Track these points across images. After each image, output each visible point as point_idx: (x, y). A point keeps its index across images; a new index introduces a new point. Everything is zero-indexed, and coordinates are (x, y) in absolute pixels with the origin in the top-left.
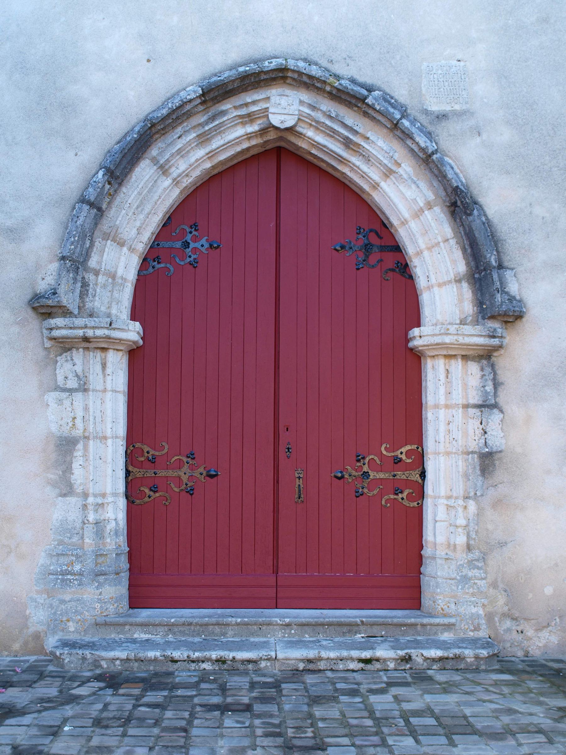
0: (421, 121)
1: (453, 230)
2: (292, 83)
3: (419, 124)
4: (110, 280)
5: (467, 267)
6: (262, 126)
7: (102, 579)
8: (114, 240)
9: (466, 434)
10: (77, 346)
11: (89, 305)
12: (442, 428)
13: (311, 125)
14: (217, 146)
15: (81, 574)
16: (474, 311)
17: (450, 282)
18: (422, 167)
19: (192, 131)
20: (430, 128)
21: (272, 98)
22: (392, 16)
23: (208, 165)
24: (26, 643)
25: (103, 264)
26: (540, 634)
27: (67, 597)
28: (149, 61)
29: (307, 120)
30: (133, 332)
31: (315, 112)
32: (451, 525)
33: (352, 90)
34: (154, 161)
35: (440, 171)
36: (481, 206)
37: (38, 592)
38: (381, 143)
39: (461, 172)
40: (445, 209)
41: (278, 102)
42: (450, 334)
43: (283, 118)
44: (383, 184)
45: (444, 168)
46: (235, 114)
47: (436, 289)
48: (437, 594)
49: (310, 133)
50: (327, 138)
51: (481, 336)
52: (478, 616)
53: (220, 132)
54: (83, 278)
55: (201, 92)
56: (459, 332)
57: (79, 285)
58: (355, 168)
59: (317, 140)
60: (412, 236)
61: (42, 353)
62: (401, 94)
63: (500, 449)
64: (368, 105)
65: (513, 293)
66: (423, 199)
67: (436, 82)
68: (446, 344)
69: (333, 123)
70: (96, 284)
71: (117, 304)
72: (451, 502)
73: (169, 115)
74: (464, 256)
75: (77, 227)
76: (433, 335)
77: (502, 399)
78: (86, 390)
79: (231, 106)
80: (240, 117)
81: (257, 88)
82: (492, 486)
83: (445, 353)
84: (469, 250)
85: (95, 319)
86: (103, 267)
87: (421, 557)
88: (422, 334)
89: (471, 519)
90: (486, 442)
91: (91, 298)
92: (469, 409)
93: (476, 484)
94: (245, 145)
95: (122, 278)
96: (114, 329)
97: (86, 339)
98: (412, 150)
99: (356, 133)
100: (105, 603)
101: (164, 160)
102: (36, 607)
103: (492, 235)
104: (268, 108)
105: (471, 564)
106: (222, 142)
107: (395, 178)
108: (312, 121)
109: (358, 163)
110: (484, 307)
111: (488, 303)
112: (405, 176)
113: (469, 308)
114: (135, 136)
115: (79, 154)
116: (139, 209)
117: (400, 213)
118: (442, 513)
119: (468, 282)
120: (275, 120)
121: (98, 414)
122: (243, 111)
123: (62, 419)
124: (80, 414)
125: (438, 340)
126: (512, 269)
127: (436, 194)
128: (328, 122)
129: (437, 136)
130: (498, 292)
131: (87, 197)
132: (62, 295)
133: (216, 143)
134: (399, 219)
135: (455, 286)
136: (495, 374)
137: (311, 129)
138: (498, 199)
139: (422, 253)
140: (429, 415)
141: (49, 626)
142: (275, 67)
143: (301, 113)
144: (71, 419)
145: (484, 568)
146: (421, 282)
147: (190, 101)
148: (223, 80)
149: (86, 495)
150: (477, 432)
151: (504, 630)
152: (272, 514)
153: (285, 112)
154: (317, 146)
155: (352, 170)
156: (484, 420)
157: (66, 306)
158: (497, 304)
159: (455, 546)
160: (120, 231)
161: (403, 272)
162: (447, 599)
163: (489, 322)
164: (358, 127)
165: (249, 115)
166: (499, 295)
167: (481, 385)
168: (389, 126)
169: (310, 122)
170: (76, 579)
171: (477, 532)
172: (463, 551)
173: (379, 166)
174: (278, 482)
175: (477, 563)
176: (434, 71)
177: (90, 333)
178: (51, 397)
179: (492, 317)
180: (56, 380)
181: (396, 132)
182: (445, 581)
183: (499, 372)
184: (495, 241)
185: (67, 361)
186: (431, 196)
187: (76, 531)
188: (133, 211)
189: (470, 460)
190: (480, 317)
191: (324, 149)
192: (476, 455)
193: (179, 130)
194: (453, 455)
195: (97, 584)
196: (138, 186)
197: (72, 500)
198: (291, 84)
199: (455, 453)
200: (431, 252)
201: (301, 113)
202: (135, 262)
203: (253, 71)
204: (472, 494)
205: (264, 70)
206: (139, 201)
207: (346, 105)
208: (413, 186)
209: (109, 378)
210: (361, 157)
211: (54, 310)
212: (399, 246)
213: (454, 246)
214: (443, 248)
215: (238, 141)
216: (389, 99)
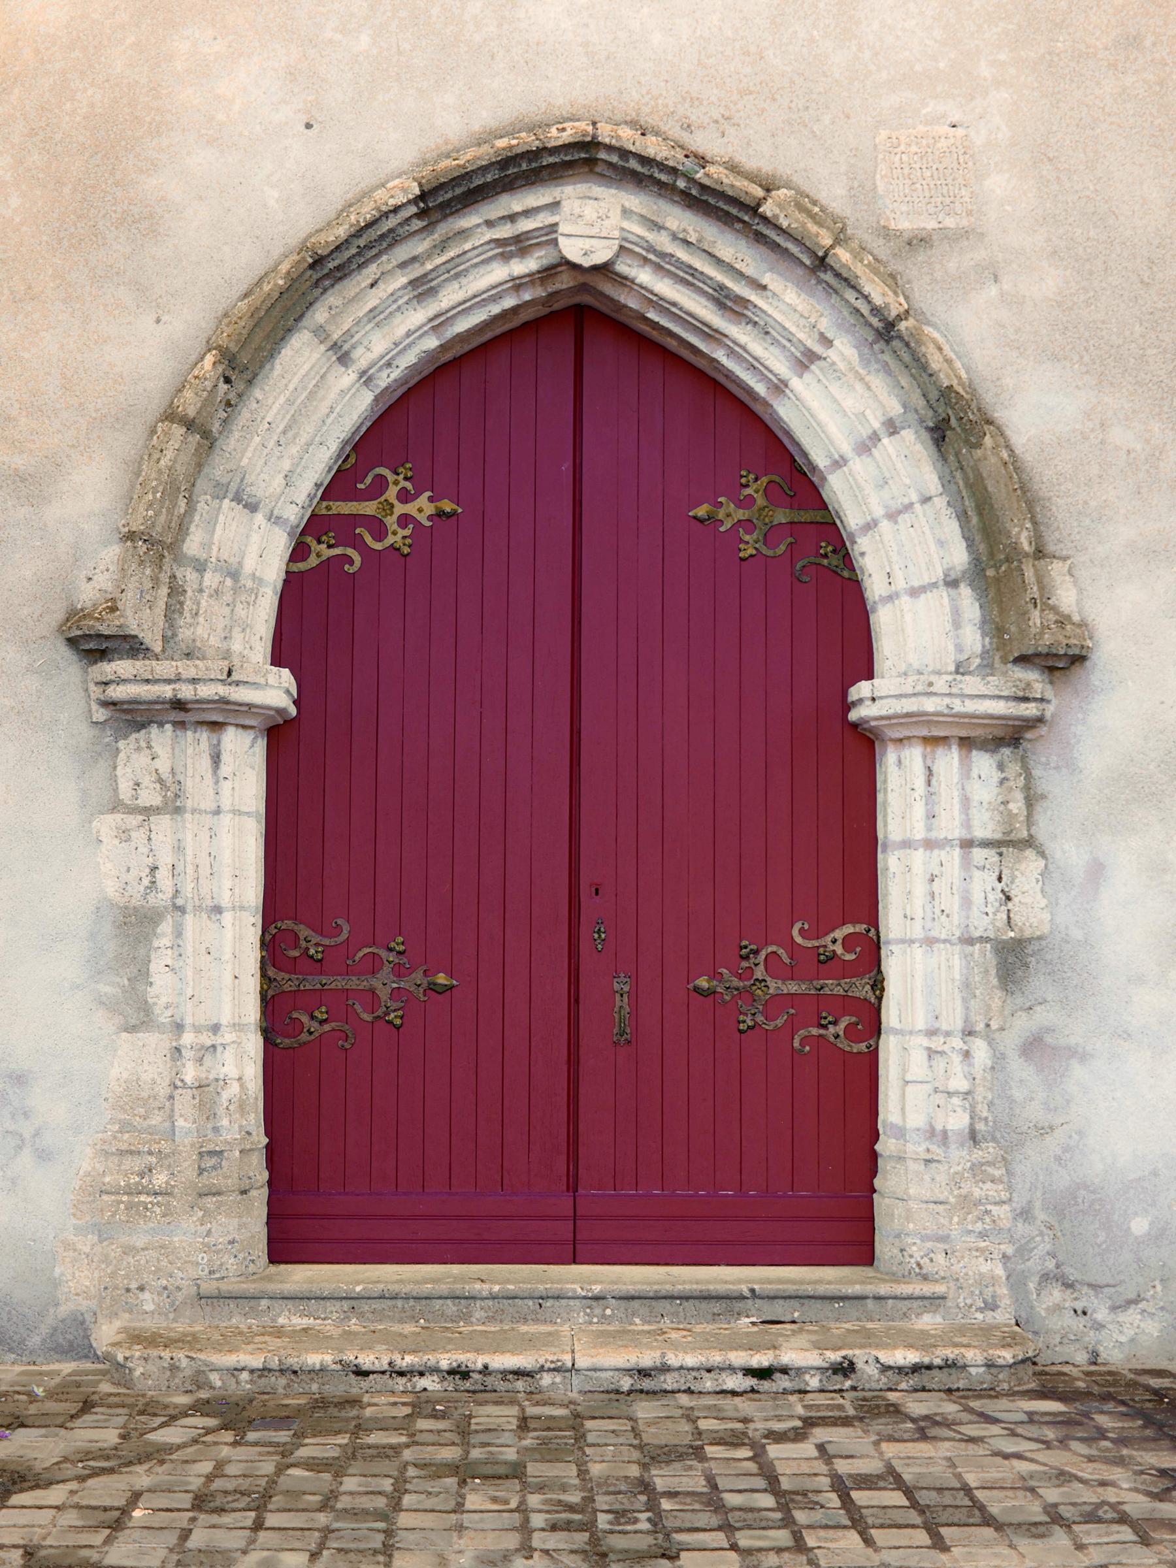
0: (875, 252)
3: (871, 258)
7: (210, 1202)
9: (967, 902)
10: (159, 718)
11: (184, 634)
12: (920, 889)
13: (646, 259)
14: (451, 303)
17: (934, 585)
20: (895, 266)
21: (564, 203)
22: (815, 33)
25: (215, 548)
26: (1122, 1317)
27: (140, 1241)
28: (308, 126)
29: (637, 249)
30: (276, 690)
34: (320, 333)
42: (935, 694)
43: (587, 244)
45: (923, 349)
46: (487, 237)
49: (643, 276)
56: (954, 690)
57: (164, 591)
58: (737, 348)
61: (87, 733)
62: (833, 194)
63: (1038, 933)
67: (906, 171)
68: (926, 714)
72: (937, 1043)
75: (160, 472)
77: (1043, 830)
80: (499, 242)
81: (533, 183)
82: (1021, 1009)
83: (924, 732)
84: (975, 520)
85: (198, 662)
86: (214, 553)
87: (874, 1156)
88: (876, 694)
89: (978, 1077)
90: (1009, 918)
91: (189, 620)
94: (509, 302)
97: (179, 705)
101: (340, 333)
103: (1021, 488)
104: (556, 224)
106: (460, 296)
107: (821, 369)
108: (648, 251)
109: (743, 339)
112: (841, 365)
114: (281, 282)
115: (164, 319)
116: (290, 434)
122: (505, 231)
126: (1065, 559)
128: (682, 254)
129: (909, 282)
132: (129, 613)
133: (450, 296)
135: (945, 594)
136: (1029, 776)
138: (1035, 413)
139: (876, 525)
142: (571, 140)
144: (148, 870)
147: (396, 210)
148: (463, 166)
149: (179, 1027)
150: (991, 897)
151: (1047, 1309)
152: (565, 1068)
155: (731, 353)
158: (1033, 630)
163: (1016, 669)
165: (517, 239)
167: (1000, 799)
168: (808, 262)
174: (577, 1001)
175: (990, 1170)
177: (186, 692)
178: (107, 825)
180: (116, 790)
181: (822, 275)
182: (924, 1206)
183: (1036, 773)
184: (1029, 501)
185: (138, 749)
186: (895, 408)
188: (276, 438)
189: (976, 956)
191: (674, 309)
193: (372, 270)
194: (942, 946)
199: (945, 941)
200: (896, 522)
204: (980, 1027)
205: (549, 145)
207: (719, 219)
208: (859, 387)
209: (226, 786)
215: (494, 293)
216: (809, 205)
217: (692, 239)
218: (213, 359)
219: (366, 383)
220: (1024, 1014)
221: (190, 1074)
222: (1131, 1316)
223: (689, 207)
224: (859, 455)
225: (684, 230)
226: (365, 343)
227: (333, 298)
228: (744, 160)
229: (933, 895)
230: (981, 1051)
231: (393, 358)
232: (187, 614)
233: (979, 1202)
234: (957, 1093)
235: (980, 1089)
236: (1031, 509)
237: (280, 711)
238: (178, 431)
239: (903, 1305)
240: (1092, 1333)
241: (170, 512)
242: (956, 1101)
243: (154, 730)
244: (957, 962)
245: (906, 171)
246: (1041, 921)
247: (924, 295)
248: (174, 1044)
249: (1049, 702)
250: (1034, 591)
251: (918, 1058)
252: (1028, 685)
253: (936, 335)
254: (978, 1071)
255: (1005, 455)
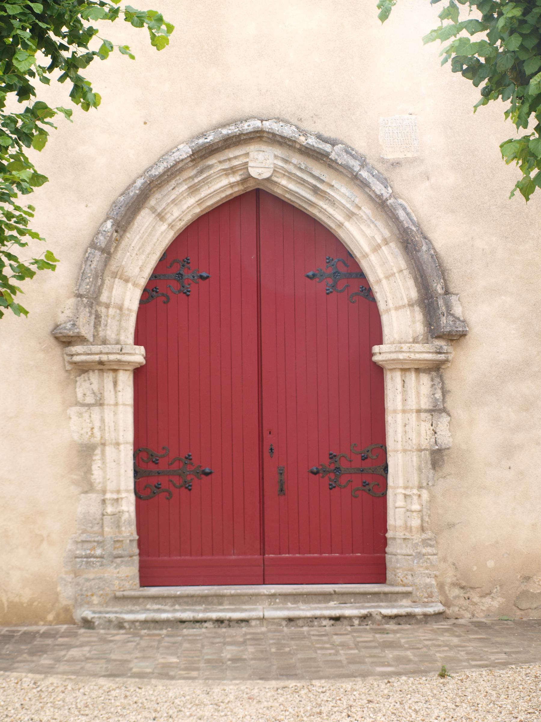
0: (378, 169)
1: (406, 262)
2: (267, 140)
3: (376, 172)
4: (118, 311)
5: (419, 293)
6: (243, 177)
7: (118, 560)
8: (121, 278)
9: (419, 434)
10: (92, 368)
11: (101, 334)
12: (400, 429)
13: (284, 175)
14: (205, 195)
15: (102, 557)
16: (424, 330)
17: (404, 306)
18: (379, 209)
19: (184, 183)
20: (386, 175)
21: (250, 153)
22: (352, 77)
23: (198, 210)
24: (58, 615)
25: (113, 299)
26: (484, 600)
27: (91, 576)
28: (145, 123)
29: (281, 171)
30: (138, 355)
31: (288, 165)
32: (408, 510)
33: (318, 148)
34: (153, 210)
35: (393, 214)
36: (430, 241)
37: (67, 573)
38: (343, 190)
39: (413, 212)
40: (399, 244)
41: (256, 157)
42: (404, 352)
43: (260, 171)
44: (347, 224)
45: (397, 212)
46: (220, 168)
47: (393, 312)
48: (398, 569)
49: (284, 182)
50: (298, 185)
51: (430, 352)
52: (431, 586)
53: (207, 183)
54: (96, 311)
55: (191, 153)
56: (411, 350)
57: (93, 317)
58: (322, 210)
59: (288, 187)
60: (372, 267)
61: (64, 375)
62: (360, 146)
63: (448, 447)
64: (331, 159)
65: (457, 315)
66: (380, 236)
67: (391, 134)
68: (400, 360)
69: (302, 173)
70: (107, 316)
71: (125, 331)
72: (408, 492)
73: (164, 173)
74: (415, 284)
75: (91, 270)
76: (390, 352)
77: (449, 405)
78: (101, 405)
79: (216, 161)
80: (224, 170)
81: (238, 145)
82: (442, 477)
83: (401, 367)
84: (420, 280)
85: (108, 346)
86: (113, 301)
87: (385, 539)
88: (381, 351)
89: (424, 505)
90: (436, 441)
91: (103, 328)
92: (422, 414)
93: (428, 477)
94: (229, 192)
95: (128, 309)
96: (124, 354)
97: (101, 363)
98: (370, 196)
99: (322, 181)
100: (122, 580)
101: (161, 209)
102: (65, 585)
103: (439, 266)
104: (248, 162)
105: (425, 543)
106: (209, 191)
107: (357, 219)
108: (285, 172)
109: (325, 206)
110: (432, 328)
111: (435, 324)
112: (365, 217)
113: (420, 328)
114: (137, 192)
115: (89, 205)
116: (141, 251)
117: (362, 248)
118: (400, 502)
119: (419, 306)
120: (254, 172)
121: (112, 425)
122: (226, 166)
123: (82, 429)
124: (97, 424)
125: (394, 356)
126: (457, 294)
127: (391, 232)
128: (299, 174)
129: (392, 181)
130: (444, 315)
131: (98, 244)
132: (81, 327)
133: (204, 192)
134: (361, 253)
135: (408, 310)
136: (443, 383)
137: (285, 178)
138: (445, 235)
139: (381, 282)
140: (389, 418)
141: (76, 600)
142: (253, 130)
143: (276, 166)
144: (90, 429)
145: (435, 545)
146: (382, 306)
147: (182, 160)
148: (209, 142)
149: (104, 492)
150: (428, 433)
151: (453, 597)
152: (259, 505)
153: (262, 165)
154: (290, 192)
155: (320, 211)
156: (434, 422)
157: (83, 336)
158: (442, 325)
159: (411, 527)
160: (125, 270)
161: (367, 296)
162: (406, 572)
163: (436, 340)
164: (324, 177)
165: (232, 168)
166: (444, 318)
167: (432, 393)
168: (350, 177)
169: (283, 172)
170: (98, 561)
171: (429, 516)
172: (418, 532)
173: (343, 209)
174: (263, 478)
175: (429, 542)
176: (389, 124)
177: (104, 358)
178: (73, 411)
179: (439, 337)
180: (76, 397)
181: (356, 182)
182: (403, 557)
183: (446, 382)
184: (442, 272)
185: (85, 380)
186: (387, 234)
187: (96, 522)
188: (135, 252)
189: (423, 456)
190: (429, 336)
191: (296, 194)
192: (427, 452)
193: (173, 183)
194: (409, 452)
195: (115, 565)
196: (139, 231)
197: (93, 496)
198: (266, 142)
199: (410, 451)
200: (389, 280)
201: (276, 166)
202: (137, 294)
203: (235, 134)
204: (425, 484)
205: (244, 132)
206: (141, 243)
207: (314, 159)
208: (372, 226)
209: (120, 394)
210: (327, 201)
211: (73, 339)
212: (363, 273)
213: (407, 276)
214: (398, 278)
215: (223, 189)
216: (351, 151)
217: (303, 167)
218: (111, 224)
219: (171, 228)
220: (442, 479)
221: (110, 509)
222: (487, 600)
223: (301, 154)
224: (373, 253)
225: (300, 164)
226: (171, 212)
227: (158, 196)
228: (323, 133)
229: (406, 432)
230: (425, 494)
231: (182, 217)
232: (102, 325)
233: (424, 555)
234: (415, 511)
235: (425, 510)
236: (443, 274)
237: (142, 363)
238: (98, 253)
239: (394, 597)
240: (471, 606)
241: (95, 285)
242: (415, 514)
243: (91, 373)
244: (415, 459)
245: (391, 134)
246: (449, 442)
247: (399, 186)
248: (102, 498)
249: (451, 353)
250: (444, 309)
251: (400, 497)
252: (441, 347)
253: (404, 203)
254: (424, 503)
255: (432, 252)
